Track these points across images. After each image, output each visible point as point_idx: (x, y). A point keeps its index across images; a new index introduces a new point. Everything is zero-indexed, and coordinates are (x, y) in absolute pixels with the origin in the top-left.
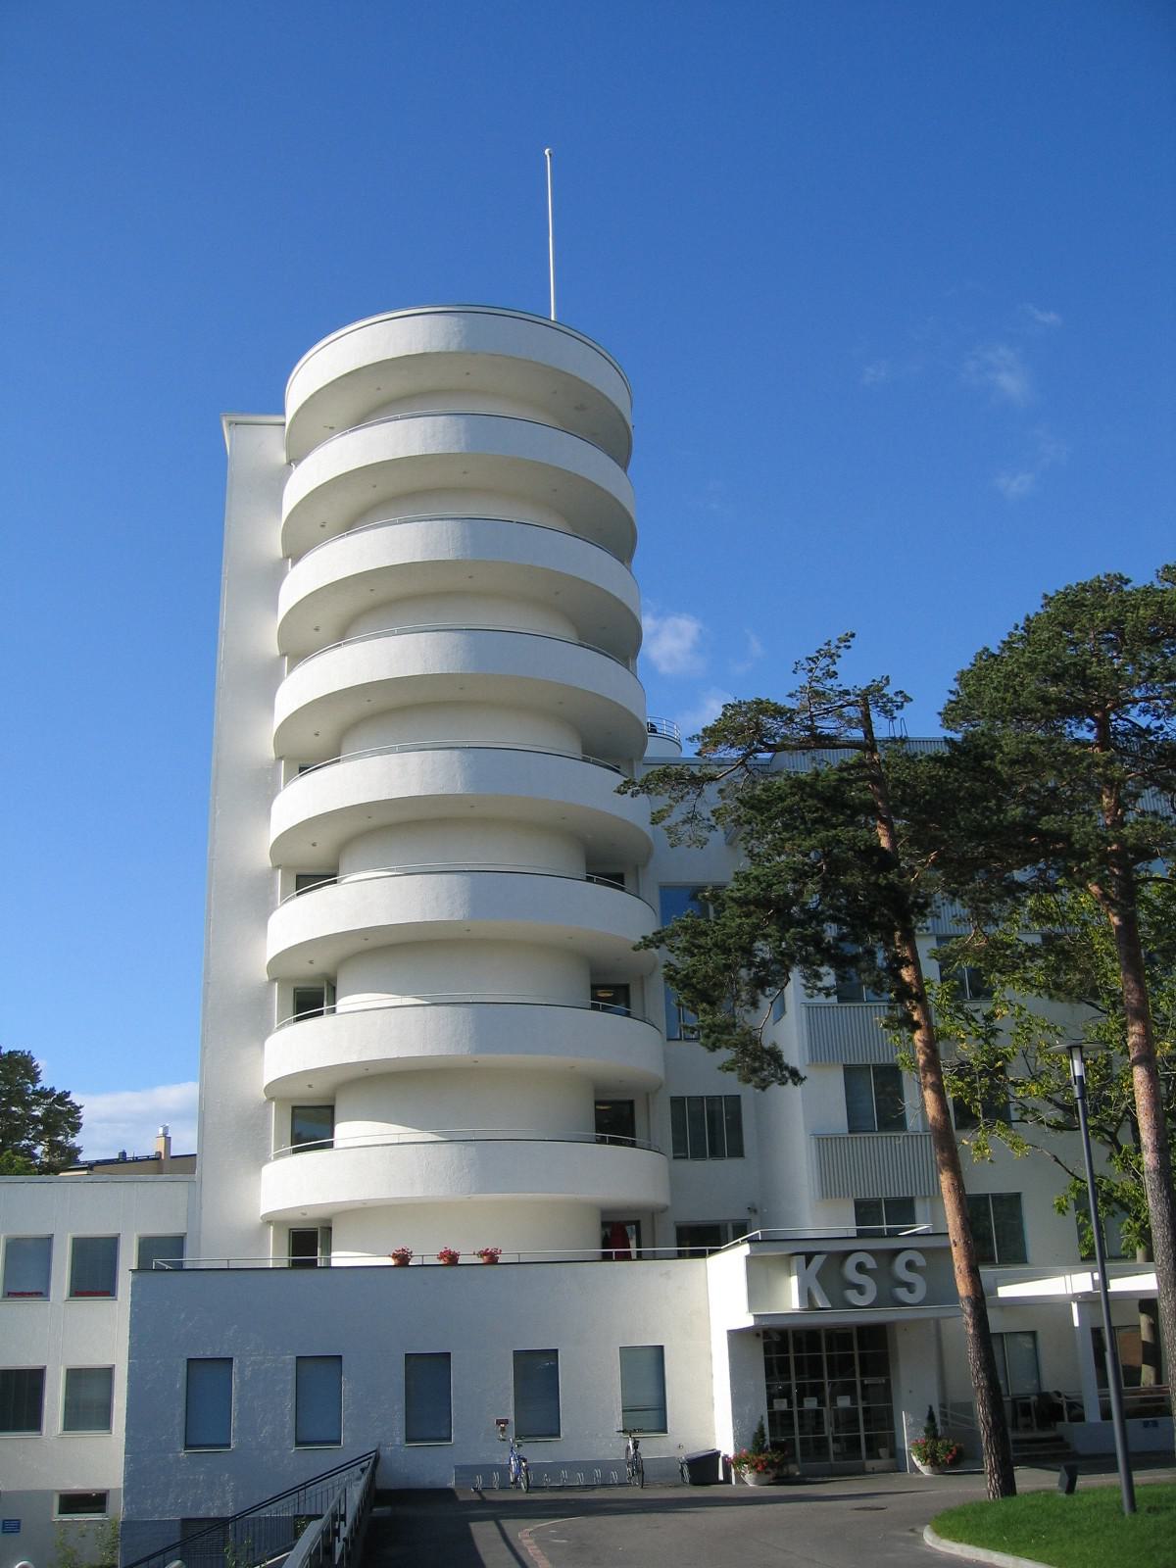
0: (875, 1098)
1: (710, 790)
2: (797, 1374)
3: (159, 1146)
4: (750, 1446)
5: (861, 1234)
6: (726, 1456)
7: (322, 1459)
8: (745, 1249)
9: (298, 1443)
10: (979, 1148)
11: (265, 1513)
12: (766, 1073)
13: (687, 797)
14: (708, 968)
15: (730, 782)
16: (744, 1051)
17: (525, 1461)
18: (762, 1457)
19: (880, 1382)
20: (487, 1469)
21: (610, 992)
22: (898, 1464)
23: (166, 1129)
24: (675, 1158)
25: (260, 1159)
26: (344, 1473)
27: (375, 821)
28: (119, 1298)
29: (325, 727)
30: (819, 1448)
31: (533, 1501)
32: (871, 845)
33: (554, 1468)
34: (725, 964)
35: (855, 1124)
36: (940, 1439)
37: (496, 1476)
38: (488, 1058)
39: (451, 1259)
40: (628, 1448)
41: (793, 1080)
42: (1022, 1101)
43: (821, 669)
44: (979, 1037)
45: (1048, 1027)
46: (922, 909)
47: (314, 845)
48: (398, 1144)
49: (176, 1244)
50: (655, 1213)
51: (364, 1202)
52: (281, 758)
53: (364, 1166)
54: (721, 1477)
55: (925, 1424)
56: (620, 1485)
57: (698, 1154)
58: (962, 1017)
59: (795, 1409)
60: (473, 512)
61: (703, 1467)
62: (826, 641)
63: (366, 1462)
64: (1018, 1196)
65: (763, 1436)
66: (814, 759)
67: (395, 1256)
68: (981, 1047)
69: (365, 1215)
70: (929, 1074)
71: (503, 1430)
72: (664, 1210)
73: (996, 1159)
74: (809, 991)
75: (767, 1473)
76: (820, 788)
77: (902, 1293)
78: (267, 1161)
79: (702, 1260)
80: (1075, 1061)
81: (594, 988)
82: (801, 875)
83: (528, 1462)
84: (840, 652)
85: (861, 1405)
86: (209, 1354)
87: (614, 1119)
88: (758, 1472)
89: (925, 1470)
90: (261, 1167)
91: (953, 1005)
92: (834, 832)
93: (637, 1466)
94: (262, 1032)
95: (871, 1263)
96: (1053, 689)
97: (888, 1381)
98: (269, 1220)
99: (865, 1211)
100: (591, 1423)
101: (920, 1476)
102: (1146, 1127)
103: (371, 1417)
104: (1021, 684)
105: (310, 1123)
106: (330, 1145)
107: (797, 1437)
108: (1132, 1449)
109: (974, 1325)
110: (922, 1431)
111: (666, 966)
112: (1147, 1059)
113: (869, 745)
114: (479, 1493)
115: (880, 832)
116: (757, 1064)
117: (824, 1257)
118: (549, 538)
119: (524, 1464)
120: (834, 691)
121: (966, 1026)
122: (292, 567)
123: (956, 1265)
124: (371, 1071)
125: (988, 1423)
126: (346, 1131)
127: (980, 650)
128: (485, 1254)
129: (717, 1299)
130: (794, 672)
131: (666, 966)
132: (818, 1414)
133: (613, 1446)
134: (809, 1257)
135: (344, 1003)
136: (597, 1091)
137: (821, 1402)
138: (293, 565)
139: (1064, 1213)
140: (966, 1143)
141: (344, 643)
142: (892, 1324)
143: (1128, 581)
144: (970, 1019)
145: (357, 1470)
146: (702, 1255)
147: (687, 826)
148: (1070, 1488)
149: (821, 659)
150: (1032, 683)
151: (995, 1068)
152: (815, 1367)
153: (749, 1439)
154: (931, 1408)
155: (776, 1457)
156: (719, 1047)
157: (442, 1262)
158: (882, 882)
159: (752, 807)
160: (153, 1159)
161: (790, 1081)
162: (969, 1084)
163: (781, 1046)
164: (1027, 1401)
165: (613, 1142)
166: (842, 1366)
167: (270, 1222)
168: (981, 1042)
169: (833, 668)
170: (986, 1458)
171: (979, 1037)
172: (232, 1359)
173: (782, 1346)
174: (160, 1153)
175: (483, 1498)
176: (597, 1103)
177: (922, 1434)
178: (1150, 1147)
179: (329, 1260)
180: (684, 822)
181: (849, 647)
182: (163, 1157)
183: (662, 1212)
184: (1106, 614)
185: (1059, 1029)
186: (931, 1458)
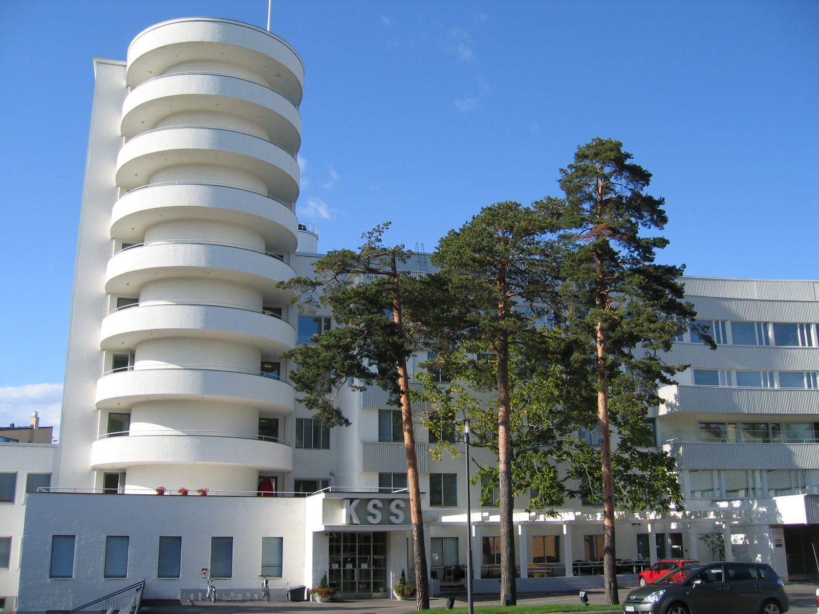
0: (392, 427)
1: (319, 289)
2: (344, 552)
3: (33, 422)
4: (319, 585)
5: (381, 491)
6: (308, 589)
7: (116, 585)
8: (323, 495)
9: (105, 577)
10: (435, 454)
11: (88, 609)
12: (334, 420)
13: (308, 291)
14: (317, 368)
15: (328, 285)
16: (325, 410)
17: (214, 588)
18: (324, 590)
19: (381, 558)
20: (196, 592)
21: (270, 366)
22: (387, 595)
23: (37, 413)
24: (296, 447)
25: (92, 438)
26: (127, 591)
27: (160, 276)
28: (16, 504)
29: (138, 226)
30: (353, 586)
31: (217, 606)
32: (387, 324)
33: (227, 592)
34: (317, 374)
35: (382, 438)
36: (406, 584)
37: (200, 594)
38: (208, 396)
39: (185, 493)
40: (263, 584)
41: (346, 424)
42: (459, 432)
43: (375, 237)
44: (442, 401)
45: (473, 399)
46: (408, 353)
47: (128, 284)
48: (162, 435)
49: (46, 479)
50: (284, 474)
51: (143, 462)
52: (113, 238)
53: (146, 445)
54: (306, 598)
55: (400, 577)
56: (258, 600)
57: (308, 446)
58: (435, 390)
59: (342, 569)
60: (213, 240)
61: (297, 594)
62: (378, 225)
63: (139, 586)
64: (455, 475)
65: (326, 580)
66: (368, 277)
67: (157, 490)
68: (443, 405)
69: (142, 468)
70: (407, 425)
71: (205, 573)
72: (289, 472)
73: (446, 459)
74: (353, 389)
75: (326, 597)
76: (367, 295)
77: (393, 519)
78: (95, 440)
79: (303, 498)
80: (466, 427)
81: (263, 363)
82: (355, 334)
83: (216, 588)
84: (384, 230)
85: (372, 568)
86: (64, 533)
87: (268, 428)
88: (322, 596)
89: (398, 598)
90: (92, 443)
91: (432, 385)
92: (371, 316)
93: (267, 593)
94: (96, 376)
95: (380, 504)
96: (477, 256)
97: (386, 558)
98: (94, 469)
99: (384, 479)
100: (247, 573)
101: (396, 600)
102: (502, 453)
103: (142, 566)
104: (464, 252)
105: (118, 423)
106: (127, 434)
107: (342, 581)
108: (474, 592)
109: (417, 536)
110: (399, 580)
111: (291, 372)
112: (506, 423)
113: (394, 275)
114: (192, 602)
115: (395, 314)
116: (330, 416)
117: (359, 500)
118: (259, 136)
119: (213, 589)
120: (380, 248)
121: (437, 395)
122: (125, 143)
123: (412, 509)
124: (150, 399)
125: (420, 578)
126: (135, 427)
127: (450, 230)
128: (201, 491)
129: (303, 524)
130: (362, 238)
131: (291, 372)
132: (353, 571)
133: (257, 583)
134: (352, 500)
135: (138, 364)
136: (260, 413)
137: (354, 566)
138: (127, 141)
139: (474, 484)
140: (431, 451)
141: (150, 186)
142: (389, 532)
143: (520, 205)
144: (439, 392)
145: (134, 590)
146: (304, 496)
147: (307, 305)
148: (451, 606)
149: (374, 232)
150: (469, 252)
151: (450, 416)
152: (353, 549)
153: (319, 581)
154: (403, 570)
155: (331, 590)
156: (313, 408)
157: (180, 494)
158: (391, 340)
159: (336, 301)
160: (28, 428)
161: (344, 424)
162: (435, 424)
163: (341, 409)
164: (450, 569)
165: (266, 439)
166: (365, 550)
167: (95, 469)
168: (443, 403)
169: (379, 237)
170: (417, 593)
171: (442, 401)
172: (75, 536)
173: (338, 540)
174: (33, 426)
175: (194, 604)
176: (260, 419)
177: (399, 582)
178: (503, 462)
179: (124, 491)
180: (306, 303)
181: (388, 228)
182: (34, 427)
183: (289, 473)
184: (506, 222)
185: (478, 401)
186: (402, 593)
